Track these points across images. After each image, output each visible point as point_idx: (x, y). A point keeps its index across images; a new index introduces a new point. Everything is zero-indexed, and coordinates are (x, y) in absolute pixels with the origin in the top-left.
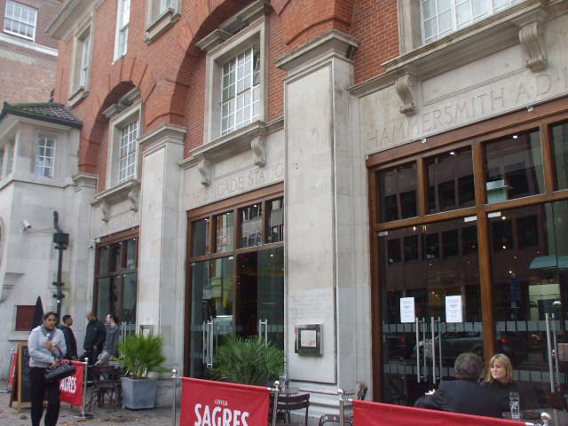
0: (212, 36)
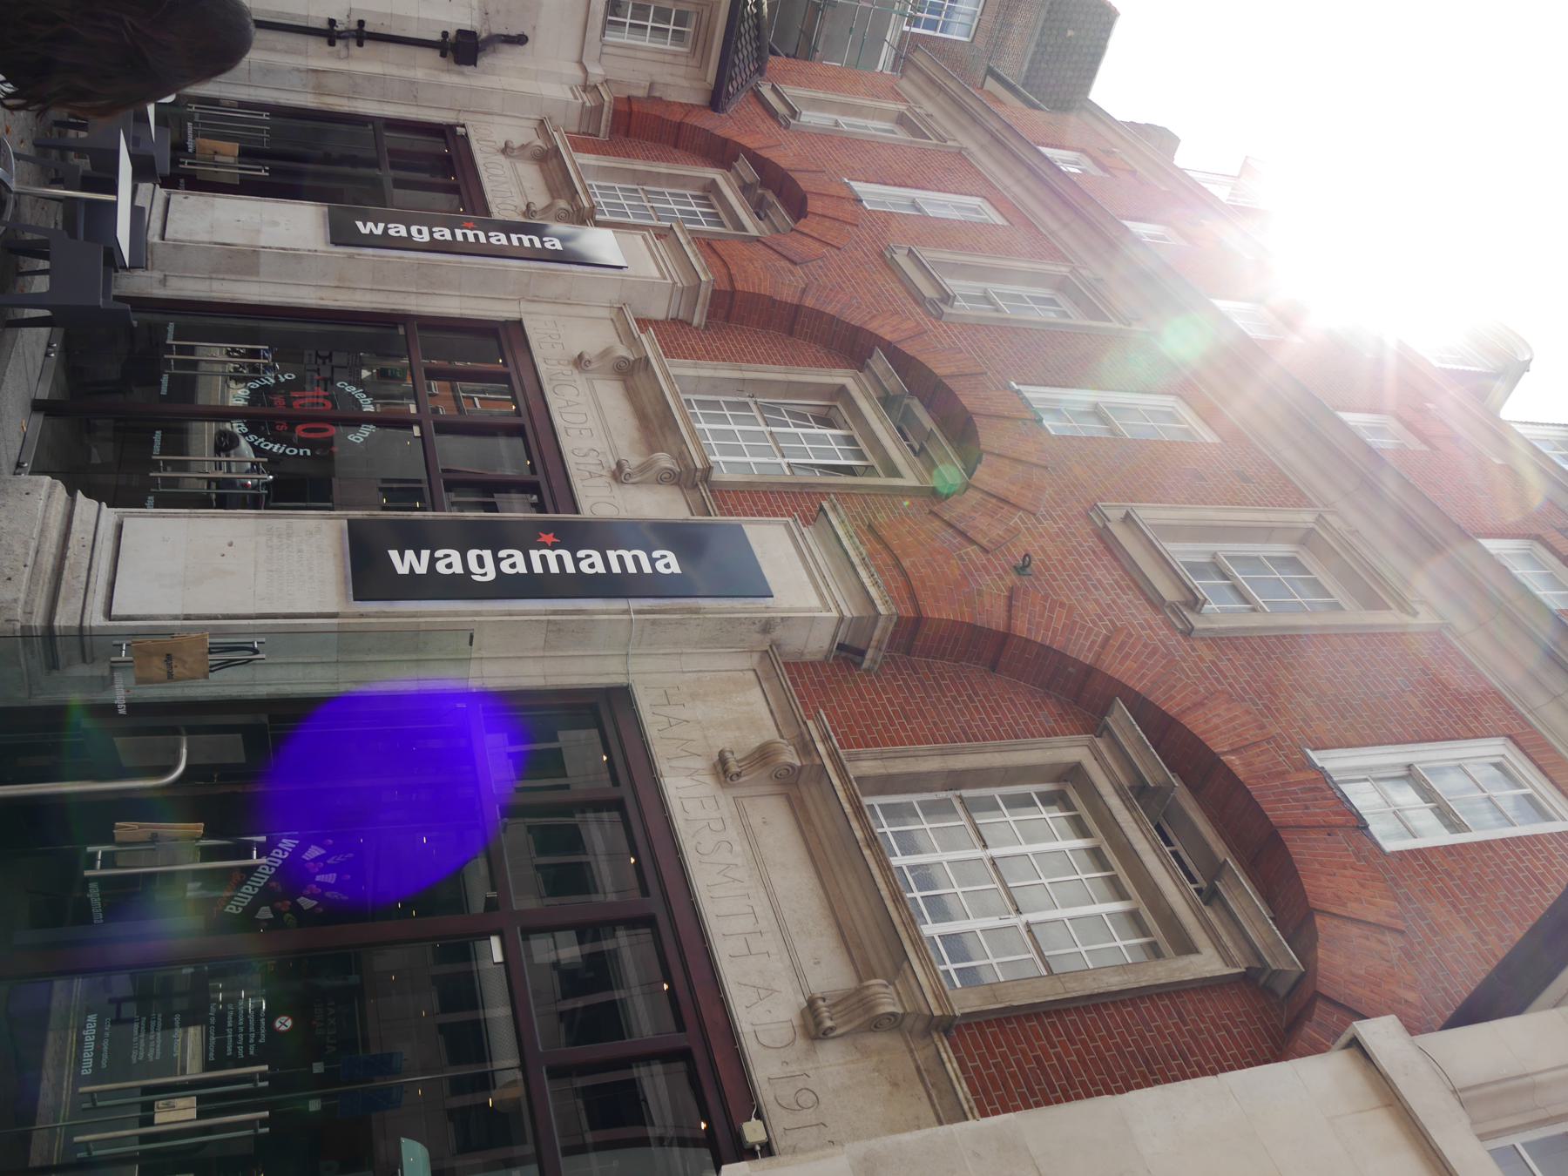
0: (894, 383)
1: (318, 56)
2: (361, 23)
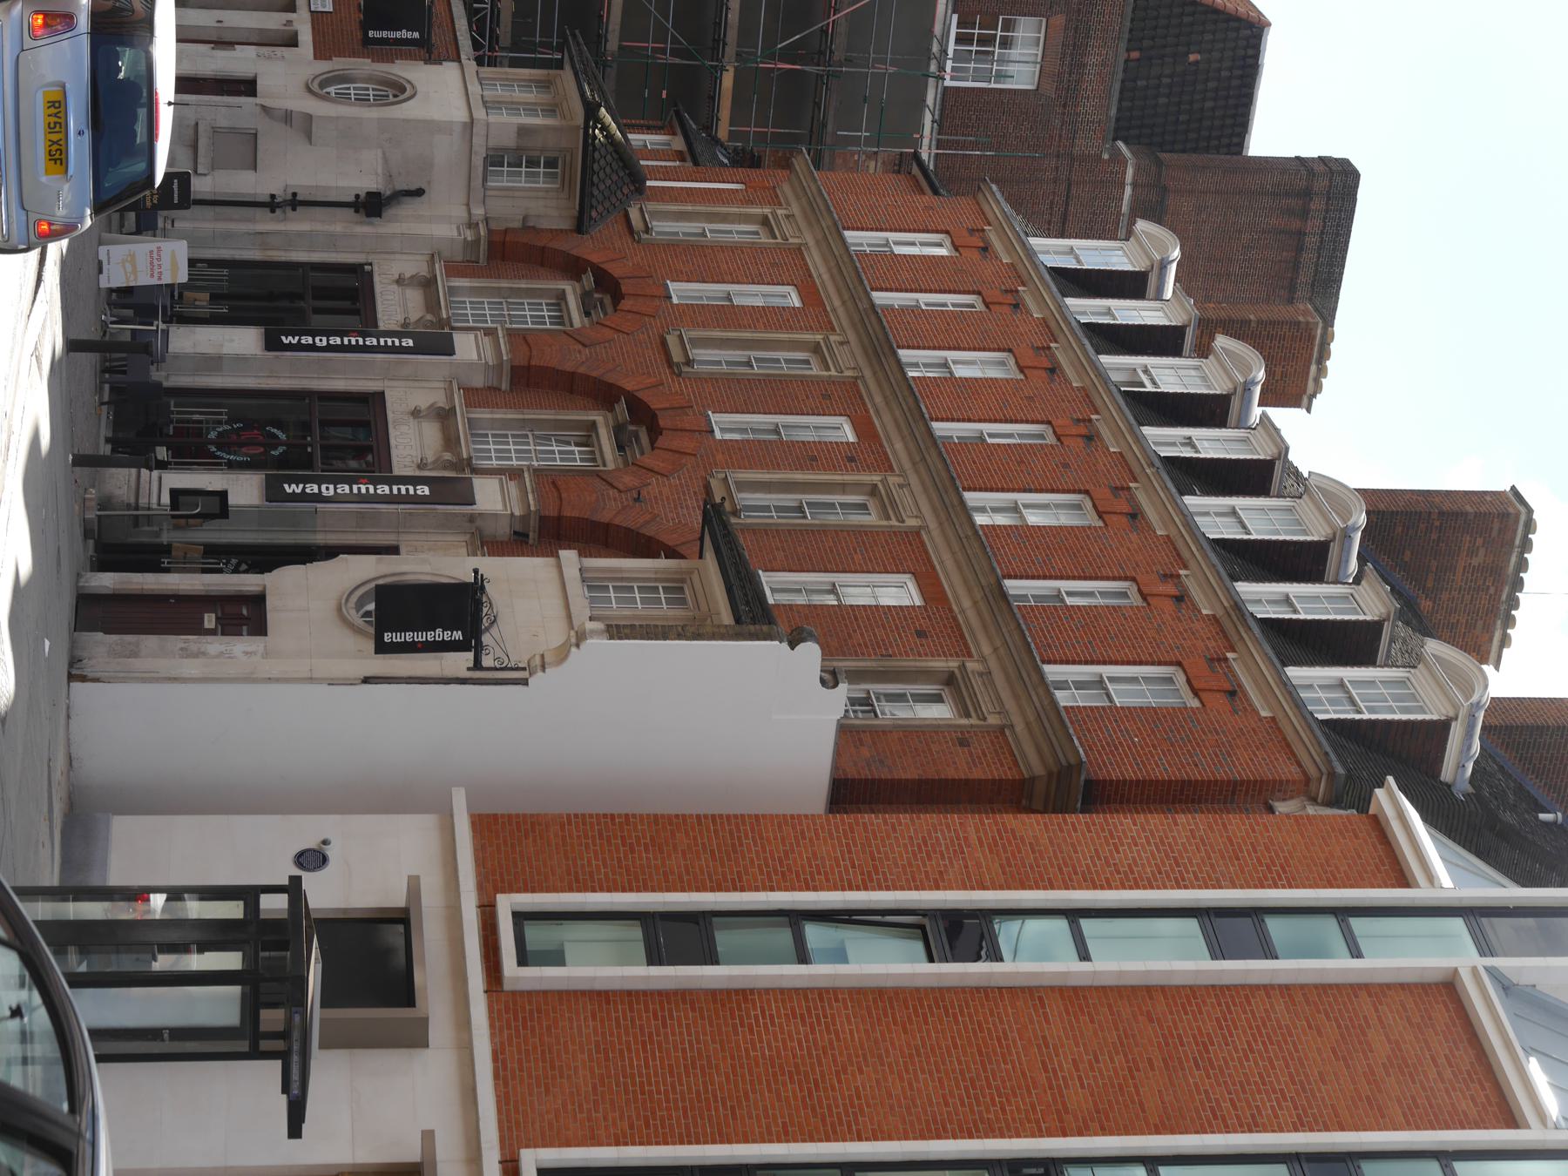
1: (266, 223)
2: (294, 194)
